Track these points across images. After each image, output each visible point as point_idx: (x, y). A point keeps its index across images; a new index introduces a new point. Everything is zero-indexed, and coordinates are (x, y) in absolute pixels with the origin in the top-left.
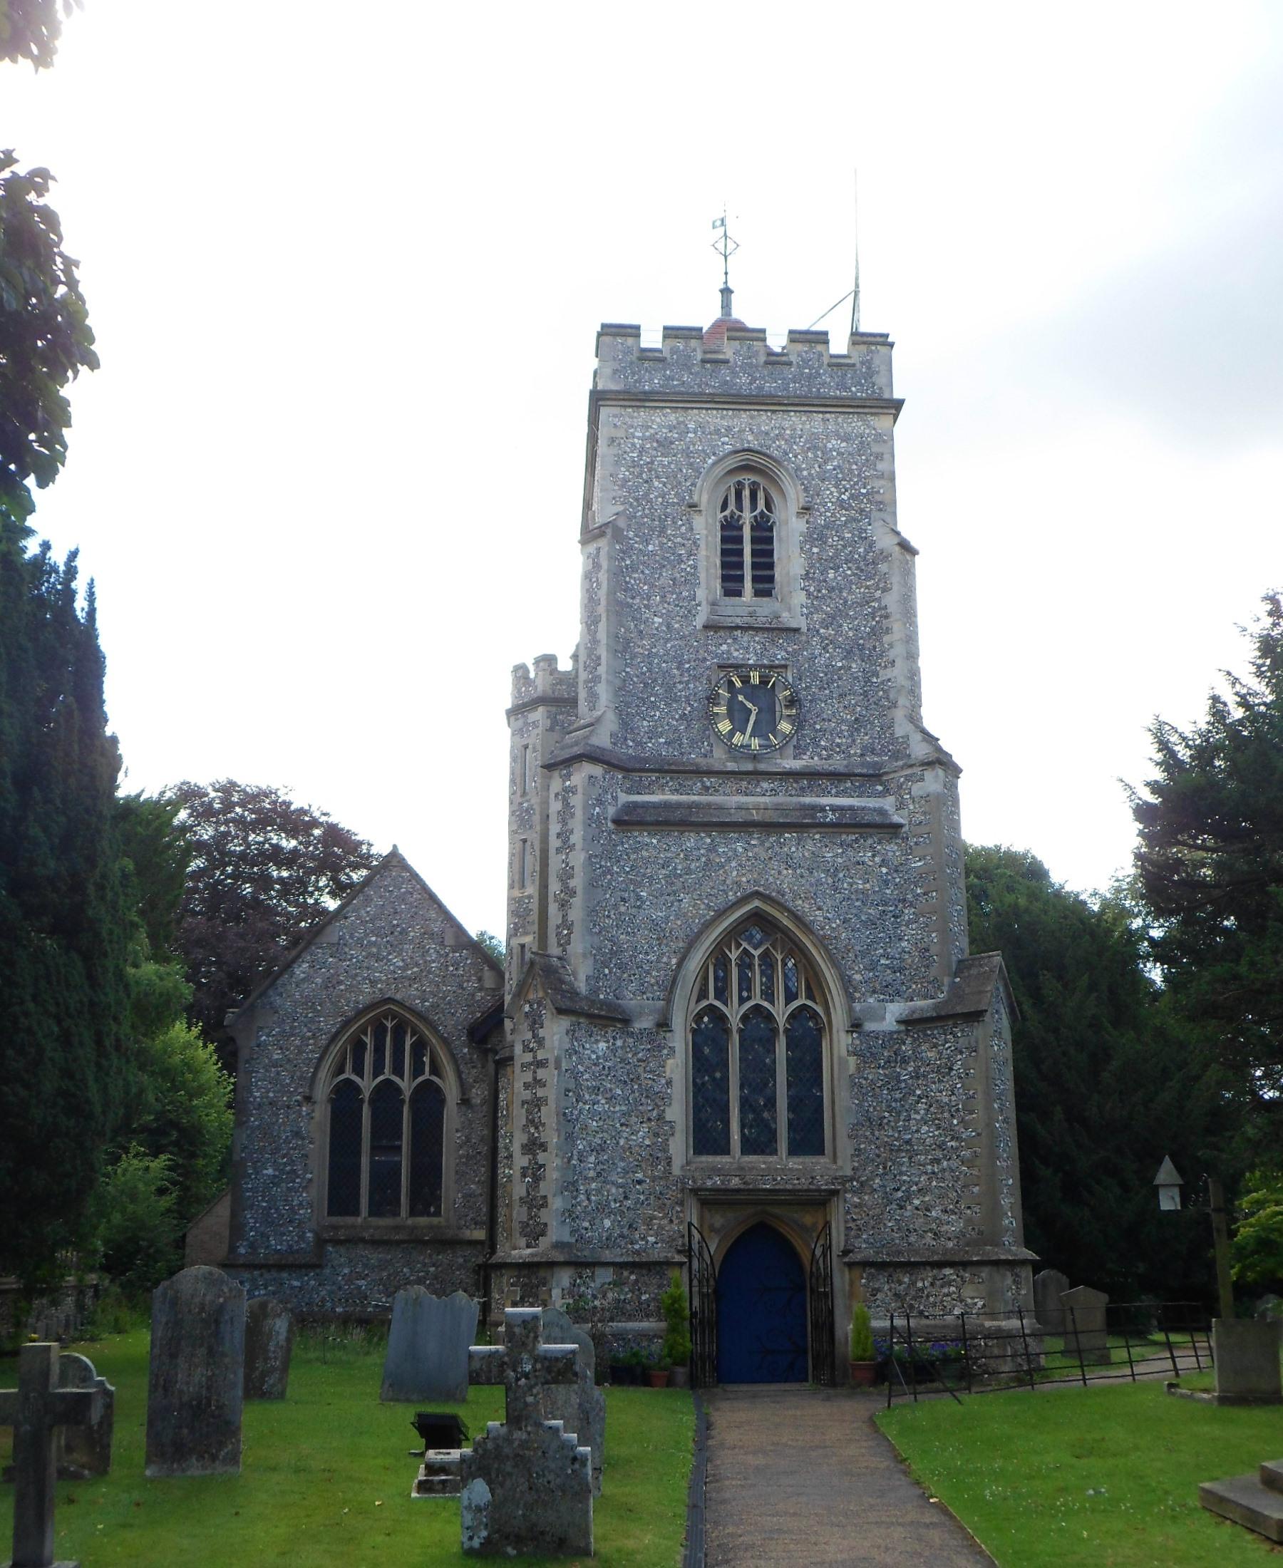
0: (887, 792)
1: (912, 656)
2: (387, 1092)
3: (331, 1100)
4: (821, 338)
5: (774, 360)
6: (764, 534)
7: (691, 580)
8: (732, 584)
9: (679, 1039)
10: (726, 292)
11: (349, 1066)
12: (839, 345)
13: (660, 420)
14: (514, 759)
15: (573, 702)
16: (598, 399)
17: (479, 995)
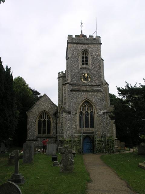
0: (101, 87)
1: (103, 72)
2: (44, 121)
3: (38, 122)
4: (93, 36)
5: (88, 39)
6: (87, 58)
7: (79, 63)
8: (83, 64)
9: (78, 115)
10: (82, 31)
11: (40, 118)
12: (95, 37)
13: (75, 46)
14: (58, 83)
15: (65, 77)
16: (68, 43)
17: (55, 110)
